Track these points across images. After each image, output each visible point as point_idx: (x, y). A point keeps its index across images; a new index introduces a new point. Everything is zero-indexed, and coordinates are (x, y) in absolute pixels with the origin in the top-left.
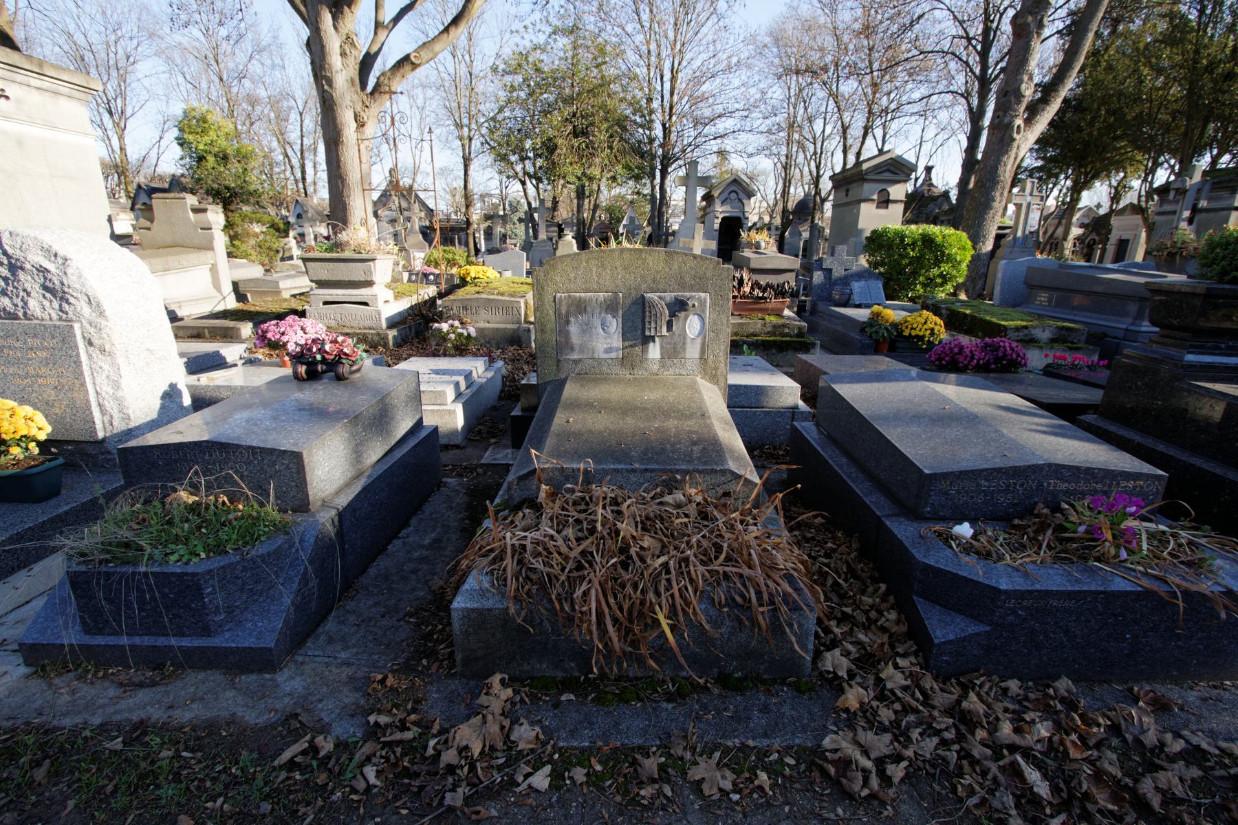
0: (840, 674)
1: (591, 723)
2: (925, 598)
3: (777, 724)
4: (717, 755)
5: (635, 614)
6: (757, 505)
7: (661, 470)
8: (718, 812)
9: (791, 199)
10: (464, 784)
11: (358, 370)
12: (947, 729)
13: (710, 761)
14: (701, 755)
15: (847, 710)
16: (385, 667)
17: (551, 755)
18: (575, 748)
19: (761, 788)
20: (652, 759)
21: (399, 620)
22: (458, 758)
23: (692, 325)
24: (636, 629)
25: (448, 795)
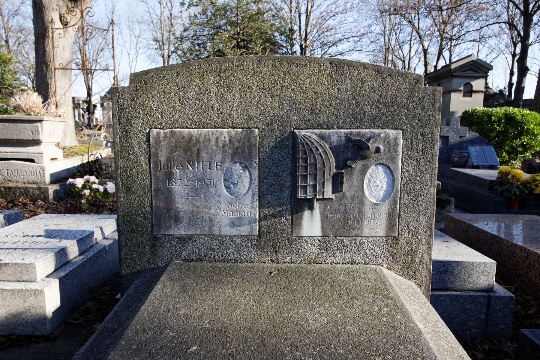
23: (375, 183)
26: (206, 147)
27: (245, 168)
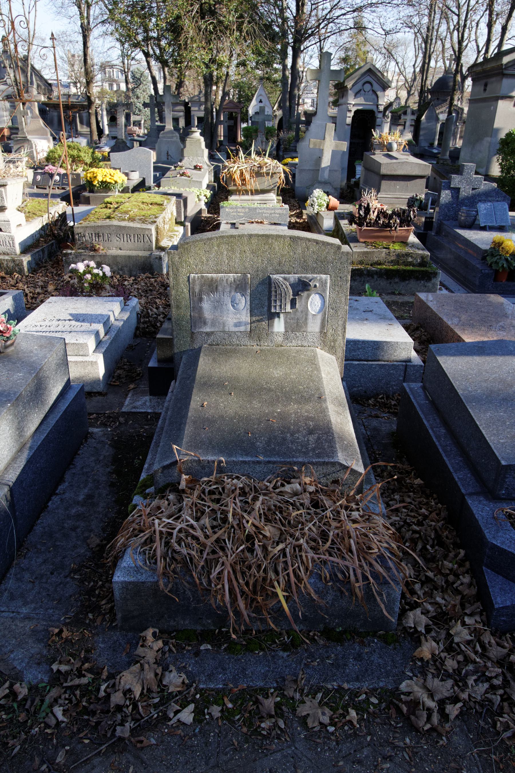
0: (419, 629)
1: (224, 669)
2: (492, 570)
3: (367, 670)
4: (319, 695)
5: (259, 588)
6: (360, 491)
7: (281, 462)
8: (318, 740)
9: (430, 78)
10: (129, 719)
11: (12, 344)
12: (496, 677)
13: (314, 701)
14: (307, 696)
15: (421, 659)
16: (59, 620)
17: (194, 695)
18: (212, 690)
19: (350, 722)
20: (270, 699)
21: (66, 577)
22: (124, 699)
23: (314, 303)
24: (259, 599)
25: (118, 728)
26: (221, 284)
27: (243, 295)
